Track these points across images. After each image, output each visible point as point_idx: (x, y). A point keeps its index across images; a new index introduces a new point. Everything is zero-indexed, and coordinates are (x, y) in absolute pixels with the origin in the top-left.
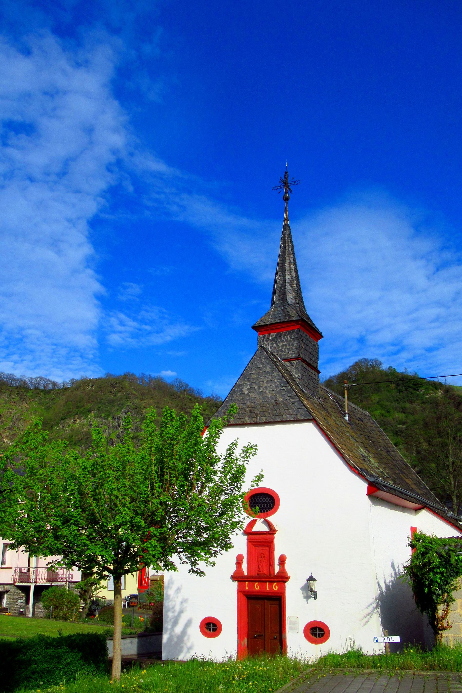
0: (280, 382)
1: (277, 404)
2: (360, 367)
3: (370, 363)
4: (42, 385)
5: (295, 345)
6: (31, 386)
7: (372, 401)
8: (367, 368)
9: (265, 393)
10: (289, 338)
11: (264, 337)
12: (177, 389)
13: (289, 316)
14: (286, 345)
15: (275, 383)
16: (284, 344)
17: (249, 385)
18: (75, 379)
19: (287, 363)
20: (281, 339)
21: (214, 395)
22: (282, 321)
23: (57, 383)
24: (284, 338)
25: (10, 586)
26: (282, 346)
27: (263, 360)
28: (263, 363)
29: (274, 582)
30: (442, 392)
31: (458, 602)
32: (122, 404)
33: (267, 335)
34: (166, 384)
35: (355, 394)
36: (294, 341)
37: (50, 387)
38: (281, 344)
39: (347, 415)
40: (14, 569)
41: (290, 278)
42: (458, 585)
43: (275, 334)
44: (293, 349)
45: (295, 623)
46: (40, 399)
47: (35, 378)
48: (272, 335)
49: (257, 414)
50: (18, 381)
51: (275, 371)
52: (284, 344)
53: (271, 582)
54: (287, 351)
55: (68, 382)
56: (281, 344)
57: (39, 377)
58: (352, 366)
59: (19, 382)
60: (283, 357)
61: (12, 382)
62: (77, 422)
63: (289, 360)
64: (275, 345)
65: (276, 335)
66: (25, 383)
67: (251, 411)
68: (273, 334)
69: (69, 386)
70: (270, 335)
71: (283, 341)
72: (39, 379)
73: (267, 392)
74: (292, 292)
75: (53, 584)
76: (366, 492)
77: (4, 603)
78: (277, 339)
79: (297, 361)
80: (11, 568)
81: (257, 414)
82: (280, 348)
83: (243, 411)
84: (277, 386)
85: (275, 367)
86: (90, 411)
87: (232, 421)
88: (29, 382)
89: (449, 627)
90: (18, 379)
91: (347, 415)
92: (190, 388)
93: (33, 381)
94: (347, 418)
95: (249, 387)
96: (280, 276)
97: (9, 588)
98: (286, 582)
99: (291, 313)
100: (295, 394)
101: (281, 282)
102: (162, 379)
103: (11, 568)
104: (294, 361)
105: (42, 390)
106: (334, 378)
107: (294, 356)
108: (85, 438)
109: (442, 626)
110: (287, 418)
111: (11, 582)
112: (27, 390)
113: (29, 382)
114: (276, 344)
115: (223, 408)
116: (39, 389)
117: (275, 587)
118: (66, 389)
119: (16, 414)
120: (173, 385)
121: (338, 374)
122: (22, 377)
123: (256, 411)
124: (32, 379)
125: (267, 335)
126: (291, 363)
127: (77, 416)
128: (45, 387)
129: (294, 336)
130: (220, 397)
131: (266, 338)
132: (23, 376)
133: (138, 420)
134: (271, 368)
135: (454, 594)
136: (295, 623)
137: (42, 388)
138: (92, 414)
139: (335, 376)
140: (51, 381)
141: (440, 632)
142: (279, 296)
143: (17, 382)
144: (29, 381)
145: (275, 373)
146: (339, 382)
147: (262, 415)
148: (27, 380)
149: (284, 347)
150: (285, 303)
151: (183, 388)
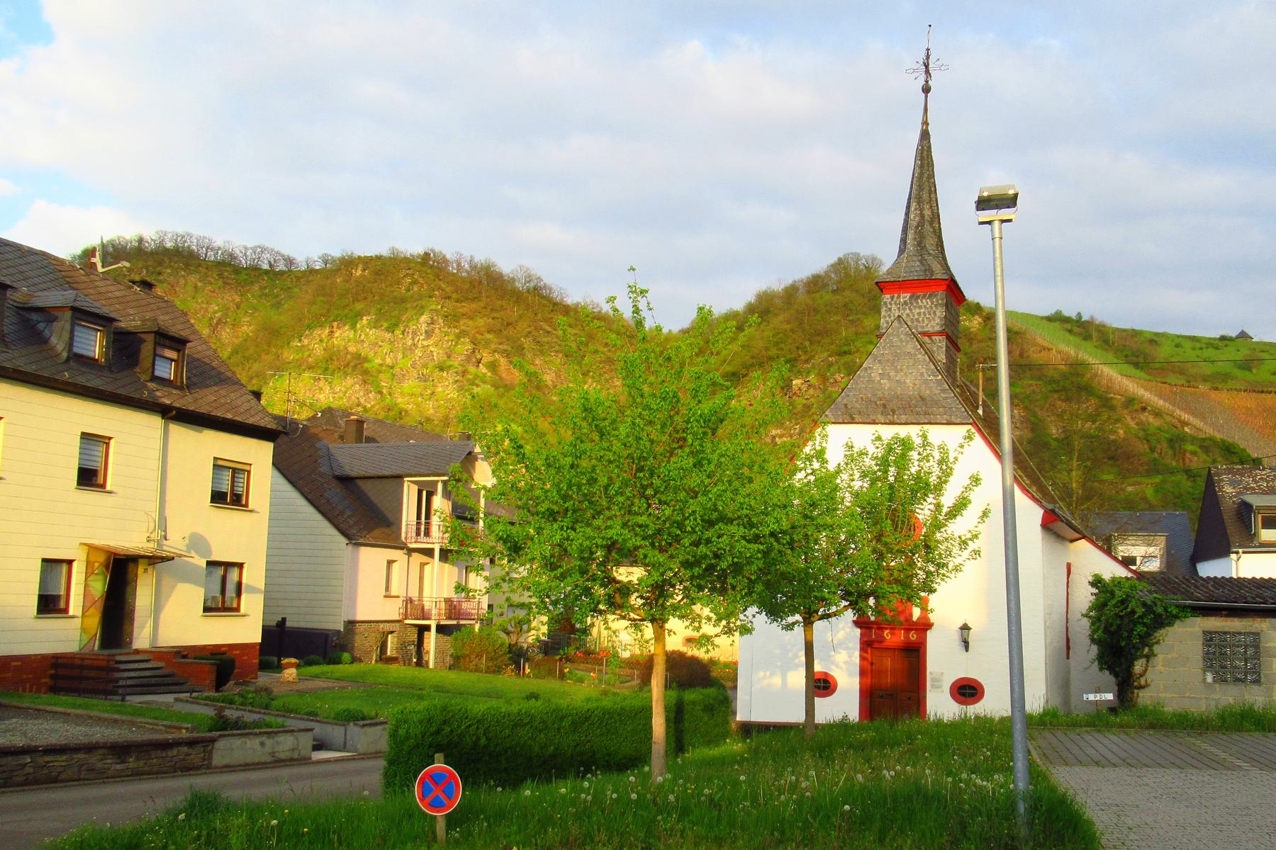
0: (927, 369)
1: (923, 399)
2: (845, 268)
3: (864, 261)
4: (266, 262)
5: (938, 314)
6: (243, 262)
7: (863, 328)
8: (857, 269)
9: (905, 382)
10: (930, 303)
11: (892, 298)
12: (520, 285)
13: (932, 272)
14: (924, 313)
15: (919, 369)
16: (922, 311)
17: (882, 369)
18: (330, 255)
19: (926, 339)
20: (918, 303)
21: (588, 300)
22: (921, 278)
23: (294, 259)
24: (922, 302)
25: (398, 625)
26: (919, 314)
27: (902, 336)
28: (901, 341)
29: (912, 629)
30: (980, 320)
31: (1160, 657)
32: (423, 307)
33: (896, 295)
34: (500, 275)
35: (836, 314)
36: (937, 308)
37: (281, 267)
38: (918, 311)
39: (981, 407)
40: (401, 599)
41: (930, 213)
42: (1161, 638)
43: (909, 295)
44: (934, 320)
45: (938, 680)
46: (262, 288)
47: (251, 248)
48: (905, 297)
49: (893, 411)
50: (220, 252)
51: (920, 353)
52: (922, 311)
53: (908, 630)
54: (926, 322)
55: (316, 259)
56: (918, 311)
57: (259, 247)
58: (832, 266)
59: (222, 254)
60: (920, 330)
61: (207, 252)
62: (337, 335)
63: (929, 335)
64: (908, 311)
65: (911, 297)
66: (232, 256)
67: (884, 406)
68: (905, 295)
69: (318, 268)
70: (902, 295)
71: (920, 307)
72: (259, 250)
73: (908, 381)
74: (933, 236)
75: (462, 622)
76: (1040, 521)
77: (428, 652)
78: (912, 304)
79: (940, 338)
80: (398, 597)
81: (893, 411)
82: (916, 317)
83: (873, 405)
84: (922, 374)
85: (919, 347)
86: (359, 315)
87: (857, 418)
88: (241, 255)
89: (1147, 685)
90: (219, 248)
91: (981, 407)
92: (545, 284)
93: (248, 253)
94: (980, 412)
95: (881, 372)
96: (916, 209)
97: (396, 627)
98: (927, 630)
99: (933, 266)
100: (947, 388)
101: (917, 219)
102: (495, 266)
103: (398, 597)
104: (937, 338)
105: (266, 272)
106: (800, 283)
107: (937, 328)
108: (352, 364)
109: (1140, 684)
110: (937, 418)
111: (396, 617)
112: (237, 270)
113: (241, 255)
114: (910, 310)
115: (843, 398)
116: (261, 269)
117: (913, 636)
118: (311, 271)
119: (216, 312)
120: (513, 278)
121: (808, 278)
122: (227, 244)
123: (890, 406)
124: (246, 249)
125: (896, 295)
126: (931, 339)
127: (335, 324)
128: (271, 265)
129: (937, 301)
130: (598, 305)
131: (895, 299)
132: (228, 242)
133: (451, 338)
134: (915, 347)
135: (1155, 648)
136: (938, 680)
137: (266, 267)
138: (365, 322)
139: (802, 280)
140: (283, 256)
141: (1136, 691)
142: (915, 239)
143: (217, 253)
144: (242, 252)
145: (920, 356)
146: (809, 292)
147: (901, 413)
148: (237, 252)
149: (922, 316)
150: (924, 252)
151: (532, 285)
